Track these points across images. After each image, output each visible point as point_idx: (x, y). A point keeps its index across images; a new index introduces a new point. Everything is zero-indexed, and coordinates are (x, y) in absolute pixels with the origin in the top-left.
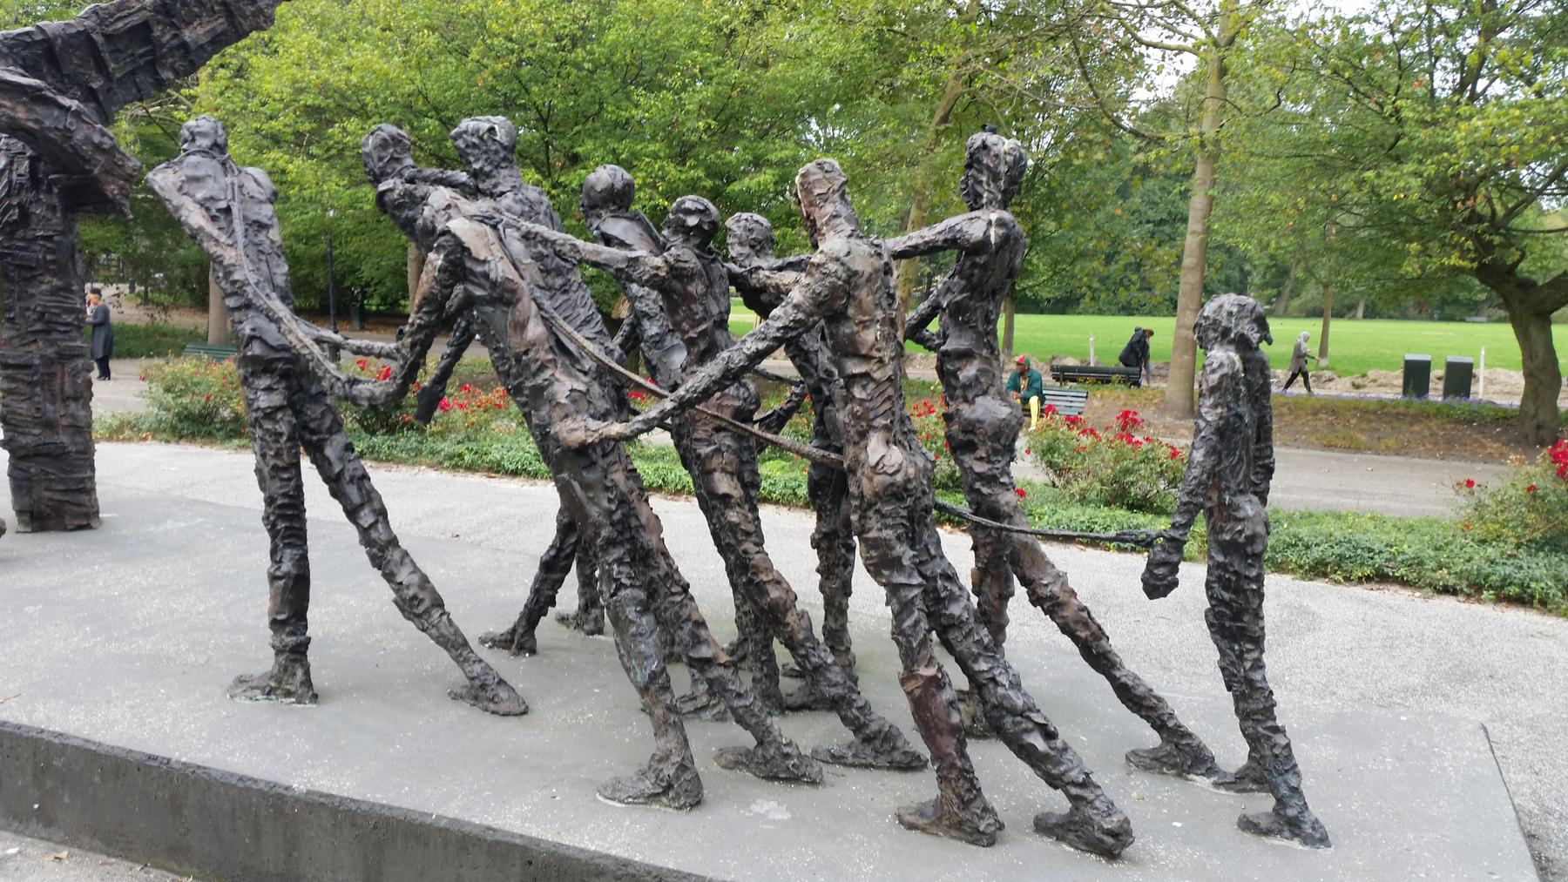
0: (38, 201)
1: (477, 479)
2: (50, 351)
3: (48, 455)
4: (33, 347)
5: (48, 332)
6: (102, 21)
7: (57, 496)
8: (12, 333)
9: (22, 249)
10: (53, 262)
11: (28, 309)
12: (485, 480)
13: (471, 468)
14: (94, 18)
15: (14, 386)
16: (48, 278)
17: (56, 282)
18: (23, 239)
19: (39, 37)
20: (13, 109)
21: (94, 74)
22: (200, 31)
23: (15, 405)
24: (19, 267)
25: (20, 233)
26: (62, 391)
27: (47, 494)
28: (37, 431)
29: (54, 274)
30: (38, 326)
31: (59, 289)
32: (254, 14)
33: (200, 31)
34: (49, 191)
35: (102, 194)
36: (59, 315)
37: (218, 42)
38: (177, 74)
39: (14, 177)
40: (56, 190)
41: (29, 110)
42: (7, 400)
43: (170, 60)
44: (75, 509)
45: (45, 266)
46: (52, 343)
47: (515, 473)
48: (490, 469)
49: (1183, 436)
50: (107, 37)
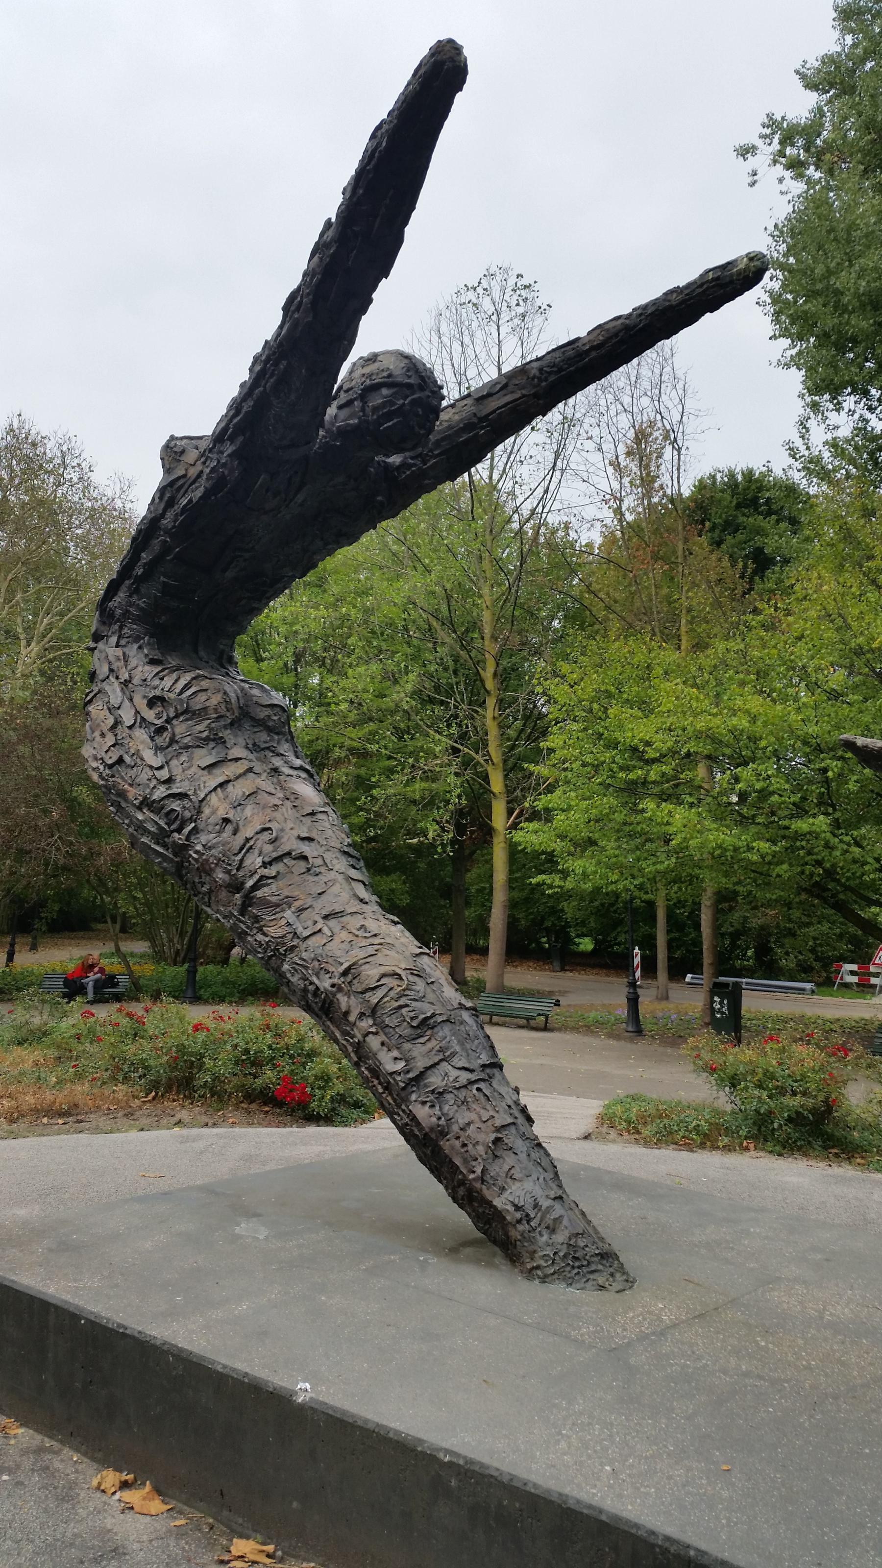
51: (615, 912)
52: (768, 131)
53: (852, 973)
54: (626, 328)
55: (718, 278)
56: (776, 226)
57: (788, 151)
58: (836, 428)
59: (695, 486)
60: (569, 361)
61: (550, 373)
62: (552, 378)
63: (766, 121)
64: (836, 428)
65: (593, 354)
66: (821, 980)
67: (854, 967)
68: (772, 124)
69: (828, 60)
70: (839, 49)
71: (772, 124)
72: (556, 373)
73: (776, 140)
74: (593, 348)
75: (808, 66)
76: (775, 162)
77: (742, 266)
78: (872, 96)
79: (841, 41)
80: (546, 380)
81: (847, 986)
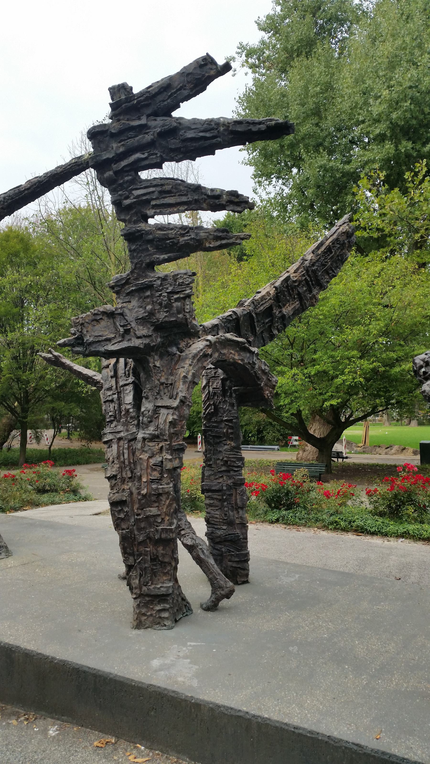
0: (225, 402)
1: (351, 537)
2: (230, 482)
3: (231, 541)
4: (221, 480)
5: (228, 471)
6: (256, 307)
7: (234, 565)
8: (210, 472)
9: (215, 427)
10: (232, 433)
11: (219, 459)
12: (355, 537)
13: (345, 530)
14: (252, 305)
15: (212, 502)
16: (229, 442)
17: (233, 444)
18: (215, 422)
19: (234, 317)
20: (234, 355)
21: (250, 334)
22: (290, 309)
23: (212, 512)
24: (214, 437)
25: (213, 419)
26: (236, 504)
27: (230, 563)
28: (224, 527)
29: (231, 439)
30: (223, 468)
31: (234, 448)
32: (311, 298)
33: (290, 309)
34: (231, 396)
35: (263, 396)
36: (235, 462)
37: (297, 313)
38: (279, 331)
39: (211, 389)
40: (234, 395)
41: (239, 355)
42: (209, 510)
43: (277, 324)
44: (242, 572)
45: (227, 436)
46: (230, 477)
47: (373, 534)
48: (356, 531)
49: (262, 468)
50: (256, 314)
51: (192, 418)
52: (240, 51)
53: (296, 440)
54: (39, 182)
55: (76, 162)
56: (239, 97)
57: (250, 60)
58: (270, 193)
59: (226, 216)
60: (16, 194)
61: (8, 199)
62: (9, 201)
63: (239, 46)
64: (270, 193)
65: (26, 192)
66: (283, 444)
67: (297, 438)
68: (242, 47)
69: (269, 17)
70: (273, 13)
71: (242, 47)
72: (11, 199)
73: (244, 55)
74: (25, 190)
75: (260, 19)
76: (243, 66)
77: (86, 157)
78: (286, 36)
79: (274, 9)
80: (7, 202)
81: (294, 446)
